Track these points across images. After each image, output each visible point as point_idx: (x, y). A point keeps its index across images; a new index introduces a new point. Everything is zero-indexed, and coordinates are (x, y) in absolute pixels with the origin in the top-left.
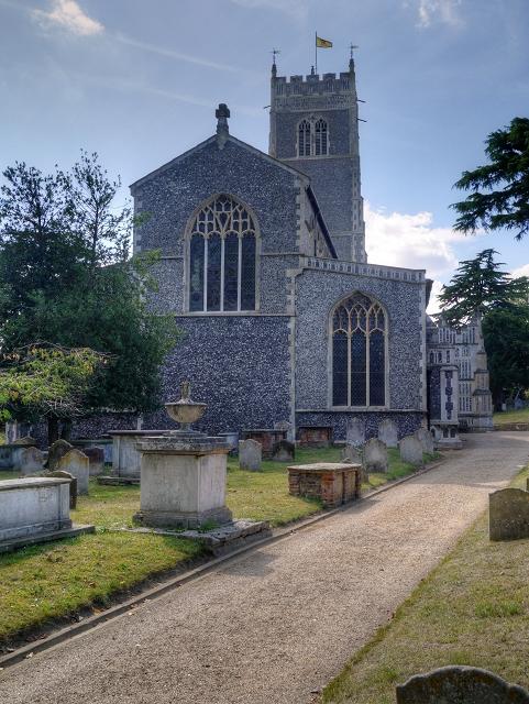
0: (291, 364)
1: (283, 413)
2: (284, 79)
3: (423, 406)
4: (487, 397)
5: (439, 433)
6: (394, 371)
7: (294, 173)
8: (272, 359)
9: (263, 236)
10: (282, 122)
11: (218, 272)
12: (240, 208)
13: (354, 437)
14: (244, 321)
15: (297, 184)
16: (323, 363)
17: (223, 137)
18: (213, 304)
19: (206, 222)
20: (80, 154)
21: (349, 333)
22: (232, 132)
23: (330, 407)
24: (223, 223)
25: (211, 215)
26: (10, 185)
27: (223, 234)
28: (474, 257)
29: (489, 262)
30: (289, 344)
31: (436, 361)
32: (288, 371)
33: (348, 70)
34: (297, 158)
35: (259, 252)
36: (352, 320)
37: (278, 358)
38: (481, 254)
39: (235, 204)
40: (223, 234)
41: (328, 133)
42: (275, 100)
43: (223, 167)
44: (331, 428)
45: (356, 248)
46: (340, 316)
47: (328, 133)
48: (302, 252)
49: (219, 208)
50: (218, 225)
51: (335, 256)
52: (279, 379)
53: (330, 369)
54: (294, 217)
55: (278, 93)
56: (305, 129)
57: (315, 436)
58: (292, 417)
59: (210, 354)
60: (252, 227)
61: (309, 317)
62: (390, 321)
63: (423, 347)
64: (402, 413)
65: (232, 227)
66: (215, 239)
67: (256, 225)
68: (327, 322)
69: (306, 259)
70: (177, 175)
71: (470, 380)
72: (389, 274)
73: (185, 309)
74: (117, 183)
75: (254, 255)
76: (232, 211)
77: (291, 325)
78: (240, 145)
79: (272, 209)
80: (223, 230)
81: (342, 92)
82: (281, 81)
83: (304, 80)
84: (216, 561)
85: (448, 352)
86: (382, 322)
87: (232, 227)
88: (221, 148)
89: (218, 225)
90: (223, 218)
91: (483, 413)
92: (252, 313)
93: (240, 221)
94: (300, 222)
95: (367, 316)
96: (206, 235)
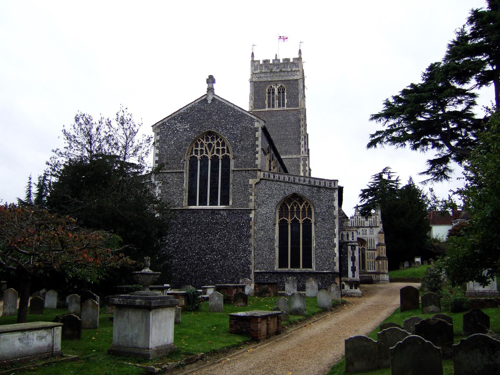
0: (252, 241)
3: (337, 268)
4: (385, 261)
5: (347, 287)
7: (255, 118)
8: (239, 237)
9: (235, 158)
10: (259, 89)
13: (290, 288)
15: (256, 125)
16: (273, 240)
19: (199, 149)
21: (289, 221)
22: (217, 92)
23: (276, 268)
27: (209, 156)
30: (250, 227)
31: (345, 239)
32: (250, 245)
33: (297, 56)
34: (267, 109)
35: (232, 168)
37: (244, 236)
39: (217, 138)
40: (209, 156)
43: (210, 114)
44: (276, 283)
45: (303, 165)
46: (283, 208)
47: (286, 94)
48: (259, 168)
49: (207, 140)
51: (286, 171)
52: (244, 250)
53: (277, 244)
54: (255, 146)
55: (255, 70)
58: (252, 276)
59: (200, 234)
60: (228, 152)
61: (263, 210)
62: (315, 213)
63: (336, 230)
65: (215, 152)
66: (204, 160)
67: (231, 149)
68: (275, 213)
69: (262, 173)
70: (182, 119)
71: (374, 250)
75: (229, 170)
76: (215, 142)
77: (252, 216)
79: (241, 140)
80: (209, 153)
82: (257, 63)
83: (271, 62)
85: (353, 233)
86: (310, 213)
88: (209, 102)
90: (210, 146)
91: (382, 271)
93: (221, 148)
94: (259, 149)
96: (199, 157)
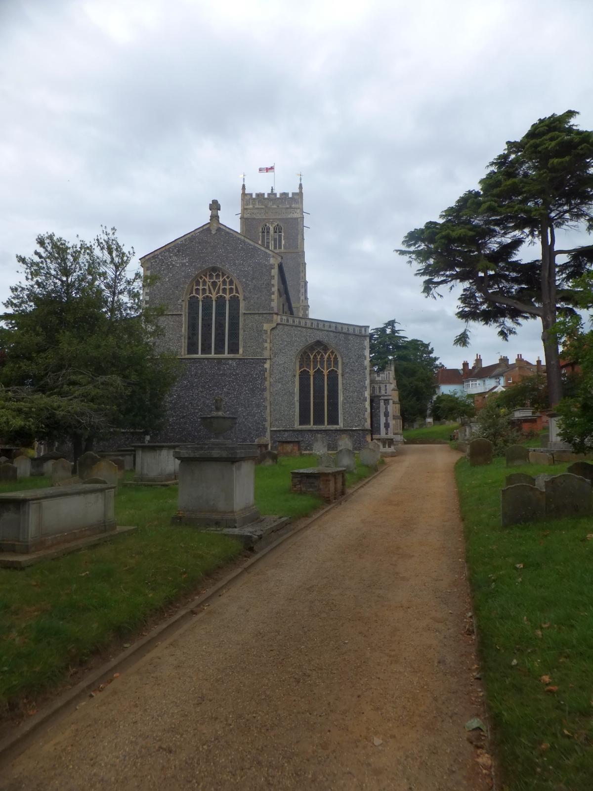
0: (267, 394)
1: (261, 432)
2: (251, 195)
3: (368, 425)
6: (345, 399)
11: (210, 325)
12: (228, 277)
14: (230, 362)
17: (215, 225)
18: (206, 349)
19: (201, 287)
20: (101, 229)
21: (312, 372)
23: (297, 426)
24: (214, 289)
25: (204, 283)
26: (41, 250)
27: (214, 296)
28: (382, 326)
29: (392, 329)
30: (265, 379)
31: (377, 393)
32: (265, 400)
33: (298, 191)
35: (242, 310)
36: (313, 361)
38: (386, 324)
39: (223, 275)
40: (214, 296)
41: (283, 234)
42: (244, 210)
46: (304, 357)
50: (210, 290)
52: (258, 406)
53: (297, 398)
56: (265, 231)
57: (289, 447)
58: (268, 434)
59: (203, 387)
60: (237, 292)
62: (343, 363)
64: (351, 430)
65: (221, 291)
69: (279, 317)
70: (178, 251)
72: (342, 328)
73: (183, 353)
74: (131, 252)
75: (239, 313)
76: (221, 280)
77: (267, 366)
78: (227, 230)
79: (253, 279)
81: (293, 206)
83: (266, 196)
84: (258, 556)
85: (386, 386)
86: (336, 363)
87: (221, 291)
88: (214, 232)
89: (210, 290)
90: (214, 284)
92: (237, 356)
93: (228, 287)
95: (325, 359)
